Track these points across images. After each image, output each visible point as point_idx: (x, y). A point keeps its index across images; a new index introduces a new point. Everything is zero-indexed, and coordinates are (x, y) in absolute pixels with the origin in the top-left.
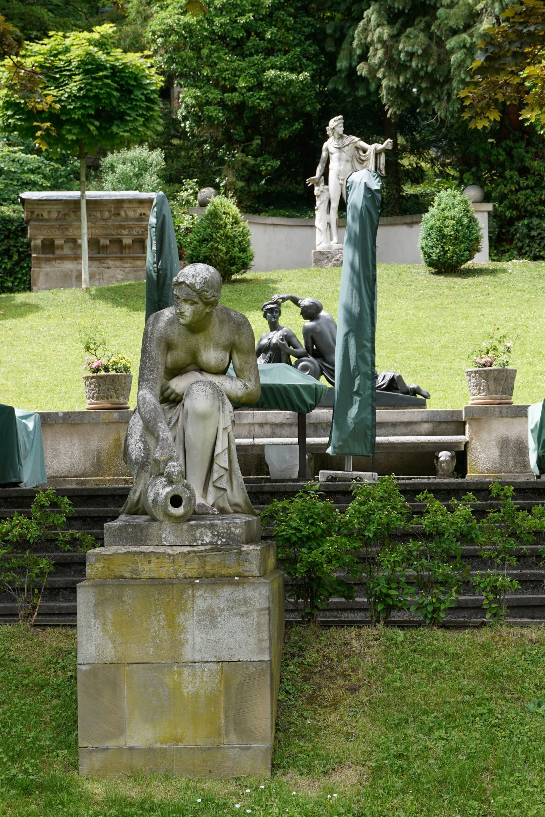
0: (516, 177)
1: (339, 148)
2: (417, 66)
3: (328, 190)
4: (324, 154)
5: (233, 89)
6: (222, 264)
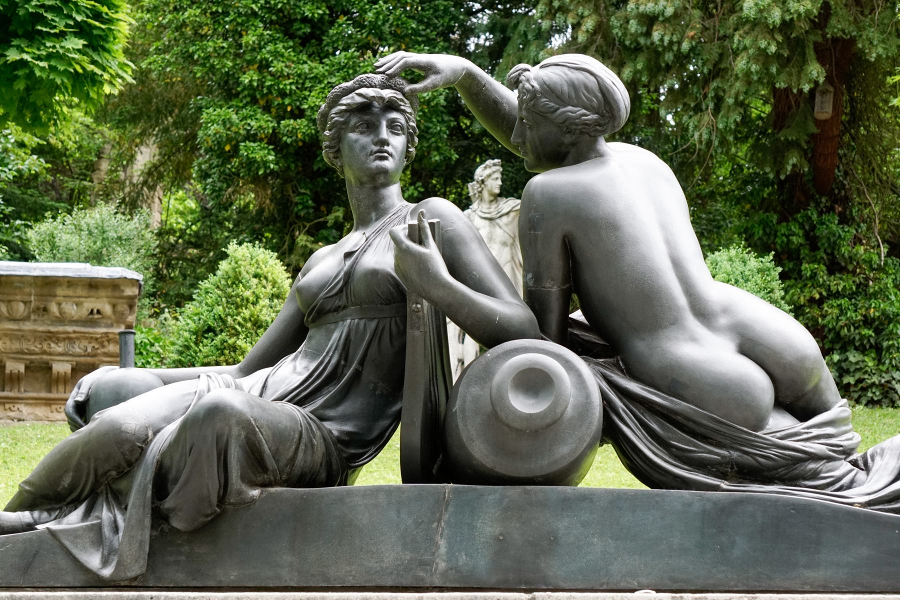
0: (823, 276)
2: (662, 40)
5: (299, 114)
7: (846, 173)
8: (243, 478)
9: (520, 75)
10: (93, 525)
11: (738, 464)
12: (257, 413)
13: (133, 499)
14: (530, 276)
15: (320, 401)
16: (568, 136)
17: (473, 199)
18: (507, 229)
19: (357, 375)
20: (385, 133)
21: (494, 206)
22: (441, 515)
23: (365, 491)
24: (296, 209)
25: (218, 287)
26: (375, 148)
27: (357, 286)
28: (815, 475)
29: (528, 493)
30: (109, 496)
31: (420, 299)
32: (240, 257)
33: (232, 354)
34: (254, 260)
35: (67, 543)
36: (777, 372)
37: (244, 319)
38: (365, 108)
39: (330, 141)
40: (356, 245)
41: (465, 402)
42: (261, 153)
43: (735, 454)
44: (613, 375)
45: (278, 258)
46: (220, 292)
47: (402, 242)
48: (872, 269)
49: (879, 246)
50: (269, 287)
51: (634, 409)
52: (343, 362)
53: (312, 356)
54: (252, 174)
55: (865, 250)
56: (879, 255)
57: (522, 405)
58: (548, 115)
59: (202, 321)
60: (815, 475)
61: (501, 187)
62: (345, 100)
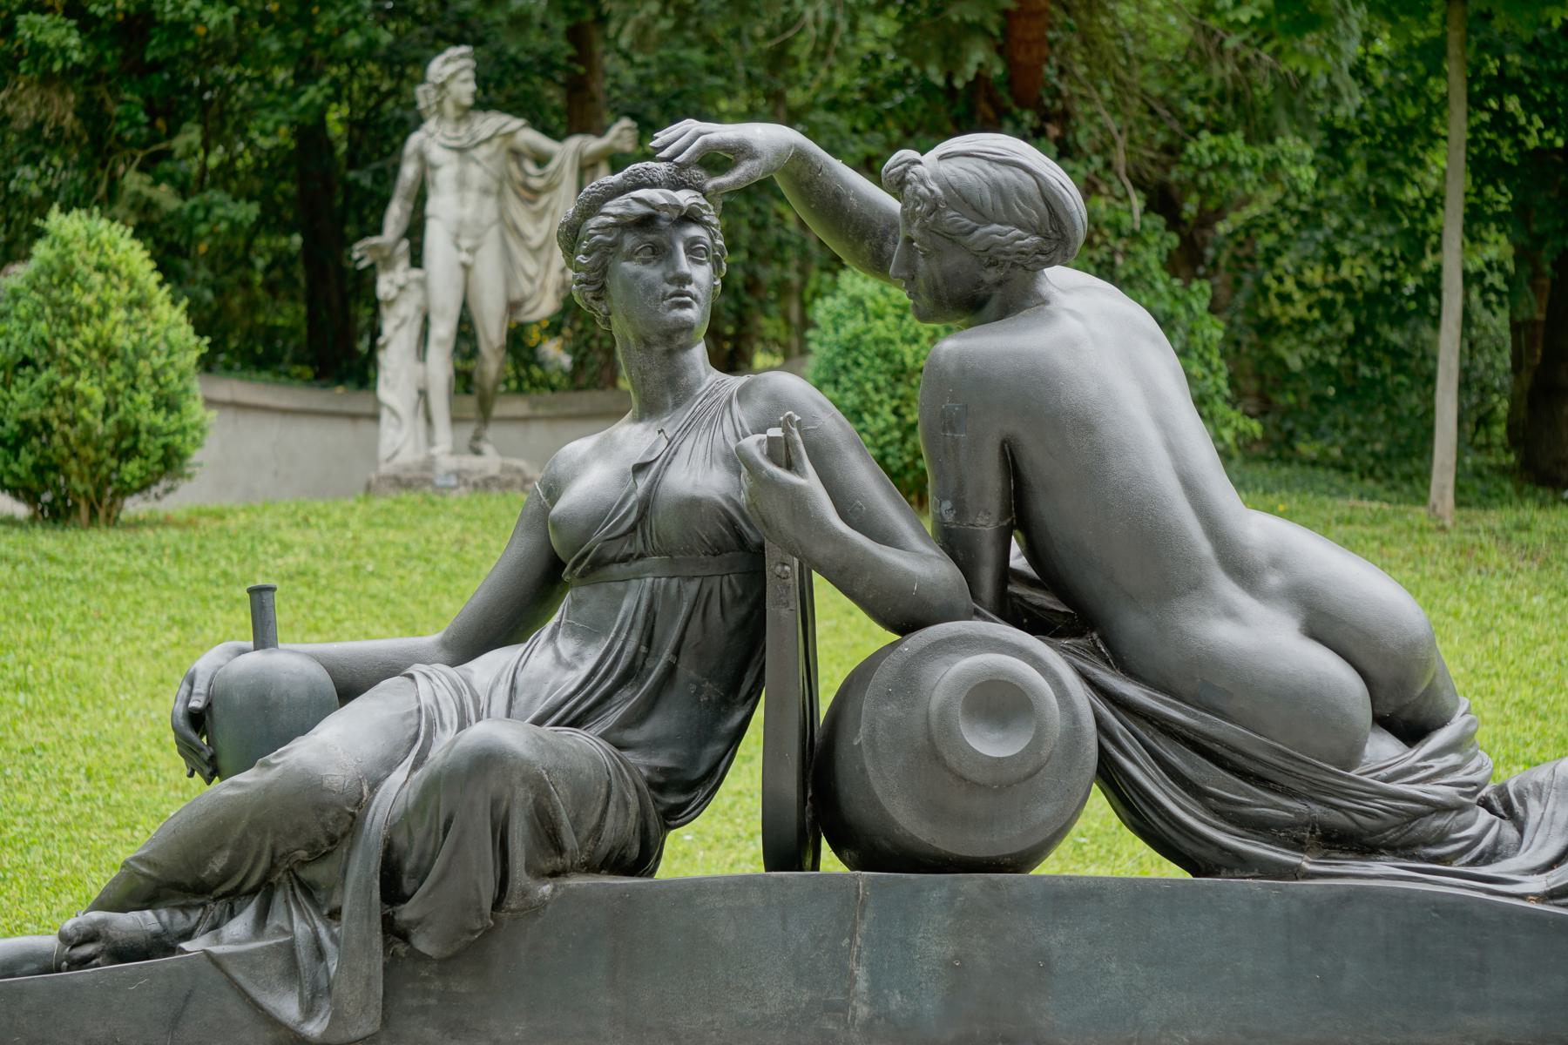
1: (461, 150)
3: (423, 283)
4: (409, 171)
6: (89, 452)
7: (1062, 71)
8: (528, 868)
9: (905, 170)
10: (279, 944)
11: (1322, 826)
12: (549, 759)
13: (348, 900)
14: (947, 505)
15: (613, 716)
16: (992, 270)
17: (426, 114)
18: (489, 166)
19: (671, 670)
20: (685, 265)
21: (462, 131)
22: (854, 926)
23: (727, 885)
24: (117, 129)
25: (34, 288)
26: (672, 289)
27: (662, 522)
28: (1442, 838)
29: (995, 885)
30: (298, 892)
31: (788, 558)
32: (70, 237)
33: (69, 404)
34: (93, 243)
35: (240, 977)
36: (1373, 668)
37: (86, 344)
38: (646, 223)
39: (588, 273)
40: (651, 451)
41: (874, 730)
42: (58, 33)
43: (1317, 810)
44: (1096, 671)
45: (135, 235)
46: (38, 297)
47: (761, 468)
48: (1119, 235)
49: (1127, 196)
50: (124, 289)
51: (1138, 730)
52: (643, 649)
53: (588, 632)
54: (40, 68)
55: (1109, 206)
56: (1130, 211)
57: (991, 745)
58: (962, 239)
59: (12, 348)
60: (1442, 838)
61: (475, 95)
62: (614, 207)
